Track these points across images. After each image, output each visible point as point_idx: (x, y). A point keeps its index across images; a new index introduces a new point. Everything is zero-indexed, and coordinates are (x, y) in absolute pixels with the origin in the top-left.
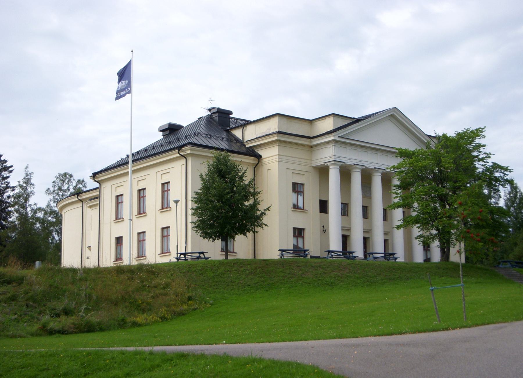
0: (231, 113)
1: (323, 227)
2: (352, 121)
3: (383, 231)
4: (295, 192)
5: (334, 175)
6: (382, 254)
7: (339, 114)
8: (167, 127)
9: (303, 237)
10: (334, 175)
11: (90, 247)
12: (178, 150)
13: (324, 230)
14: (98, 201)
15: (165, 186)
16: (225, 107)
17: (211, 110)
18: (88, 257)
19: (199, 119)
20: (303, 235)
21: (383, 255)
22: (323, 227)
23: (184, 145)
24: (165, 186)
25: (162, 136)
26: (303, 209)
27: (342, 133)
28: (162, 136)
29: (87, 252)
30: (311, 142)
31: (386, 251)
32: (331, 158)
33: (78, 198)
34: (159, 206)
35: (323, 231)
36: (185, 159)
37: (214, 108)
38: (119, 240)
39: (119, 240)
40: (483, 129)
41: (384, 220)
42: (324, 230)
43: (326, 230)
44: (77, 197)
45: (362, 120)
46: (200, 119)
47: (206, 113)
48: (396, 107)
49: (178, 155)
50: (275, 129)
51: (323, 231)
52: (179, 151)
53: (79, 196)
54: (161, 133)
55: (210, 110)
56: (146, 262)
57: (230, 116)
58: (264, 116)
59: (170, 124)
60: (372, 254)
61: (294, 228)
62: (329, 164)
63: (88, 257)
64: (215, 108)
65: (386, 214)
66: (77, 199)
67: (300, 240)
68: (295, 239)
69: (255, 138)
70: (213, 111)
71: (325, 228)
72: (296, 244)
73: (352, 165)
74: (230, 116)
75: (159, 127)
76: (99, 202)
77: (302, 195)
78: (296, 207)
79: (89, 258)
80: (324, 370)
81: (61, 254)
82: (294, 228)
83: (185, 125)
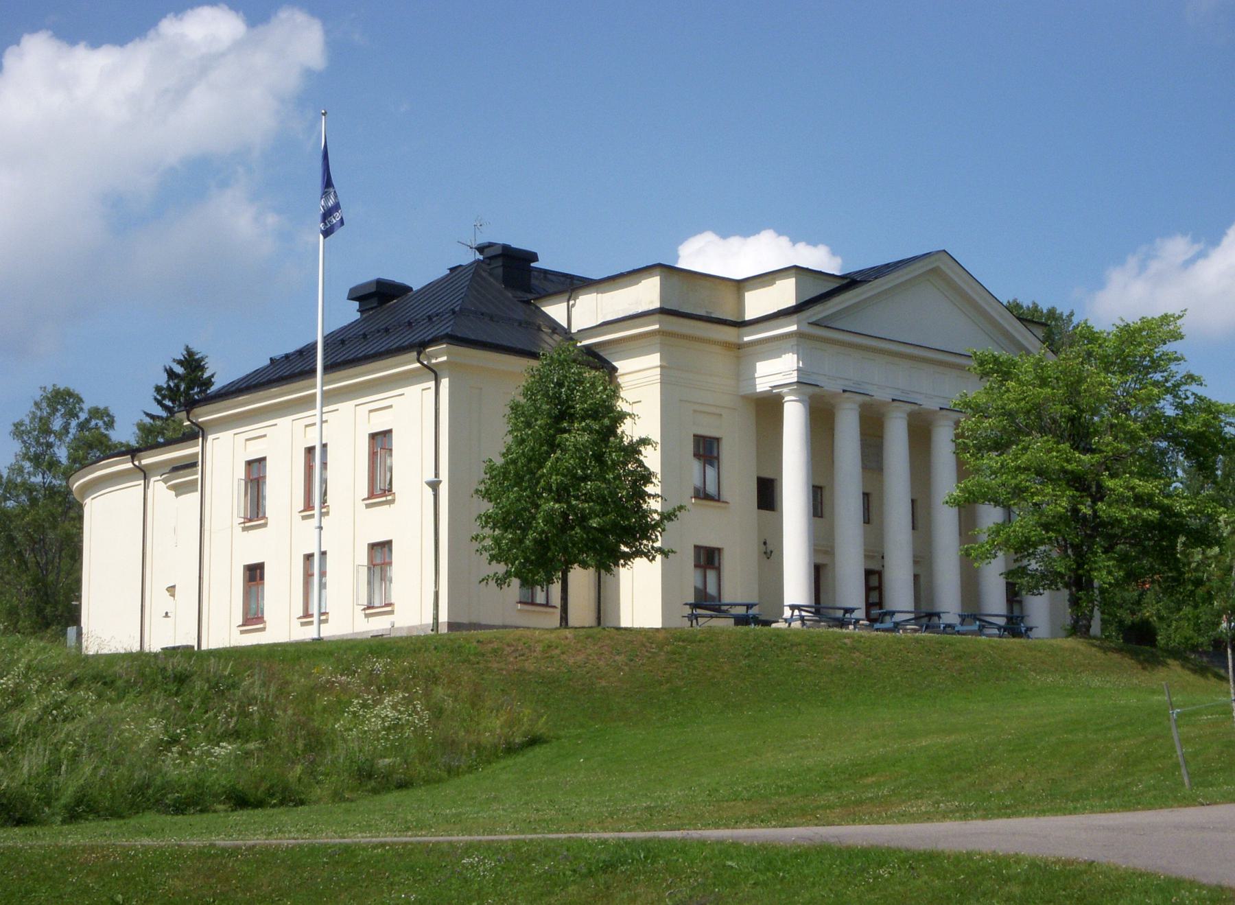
0: (533, 257)
1: (765, 543)
2: (838, 285)
3: (862, 552)
4: (699, 459)
5: (794, 416)
6: (990, 621)
7: (823, 271)
8: (373, 290)
9: (718, 570)
10: (794, 416)
11: (174, 587)
12: (415, 353)
13: (768, 551)
14: (197, 474)
15: (380, 441)
16: (519, 242)
17: (486, 250)
18: (167, 613)
19: (452, 270)
20: (717, 564)
21: (912, 616)
22: (765, 543)
23: (434, 341)
24: (380, 441)
25: (358, 311)
26: (718, 500)
27: (818, 312)
28: (358, 311)
29: (158, 600)
30: (740, 336)
31: (822, 596)
32: (788, 376)
33: (133, 462)
34: (364, 491)
35: (765, 553)
36: (433, 374)
37: (491, 245)
38: (254, 573)
39: (254, 573)
40: (1180, 317)
41: (864, 523)
42: (770, 552)
43: (771, 552)
44: (130, 460)
45: (860, 281)
46: (456, 272)
47: (468, 257)
48: (944, 251)
49: (418, 365)
50: (652, 302)
51: (765, 553)
52: (419, 354)
53: (136, 459)
54: (356, 304)
55: (481, 249)
56: (330, 631)
57: (532, 265)
58: (623, 271)
59: (380, 283)
60: (892, 613)
61: (696, 547)
62: (785, 390)
63: (167, 613)
64: (495, 244)
65: (868, 506)
66: (130, 465)
67: (711, 575)
68: (699, 572)
69: (598, 323)
70: (490, 252)
71: (770, 547)
72: (700, 585)
73: (888, 403)
74: (532, 265)
75: (351, 290)
76: (199, 476)
77: (716, 467)
78: (702, 495)
79: (169, 615)
80: (1124, 866)
81: (77, 603)
82: (696, 547)
83: (416, 285)
